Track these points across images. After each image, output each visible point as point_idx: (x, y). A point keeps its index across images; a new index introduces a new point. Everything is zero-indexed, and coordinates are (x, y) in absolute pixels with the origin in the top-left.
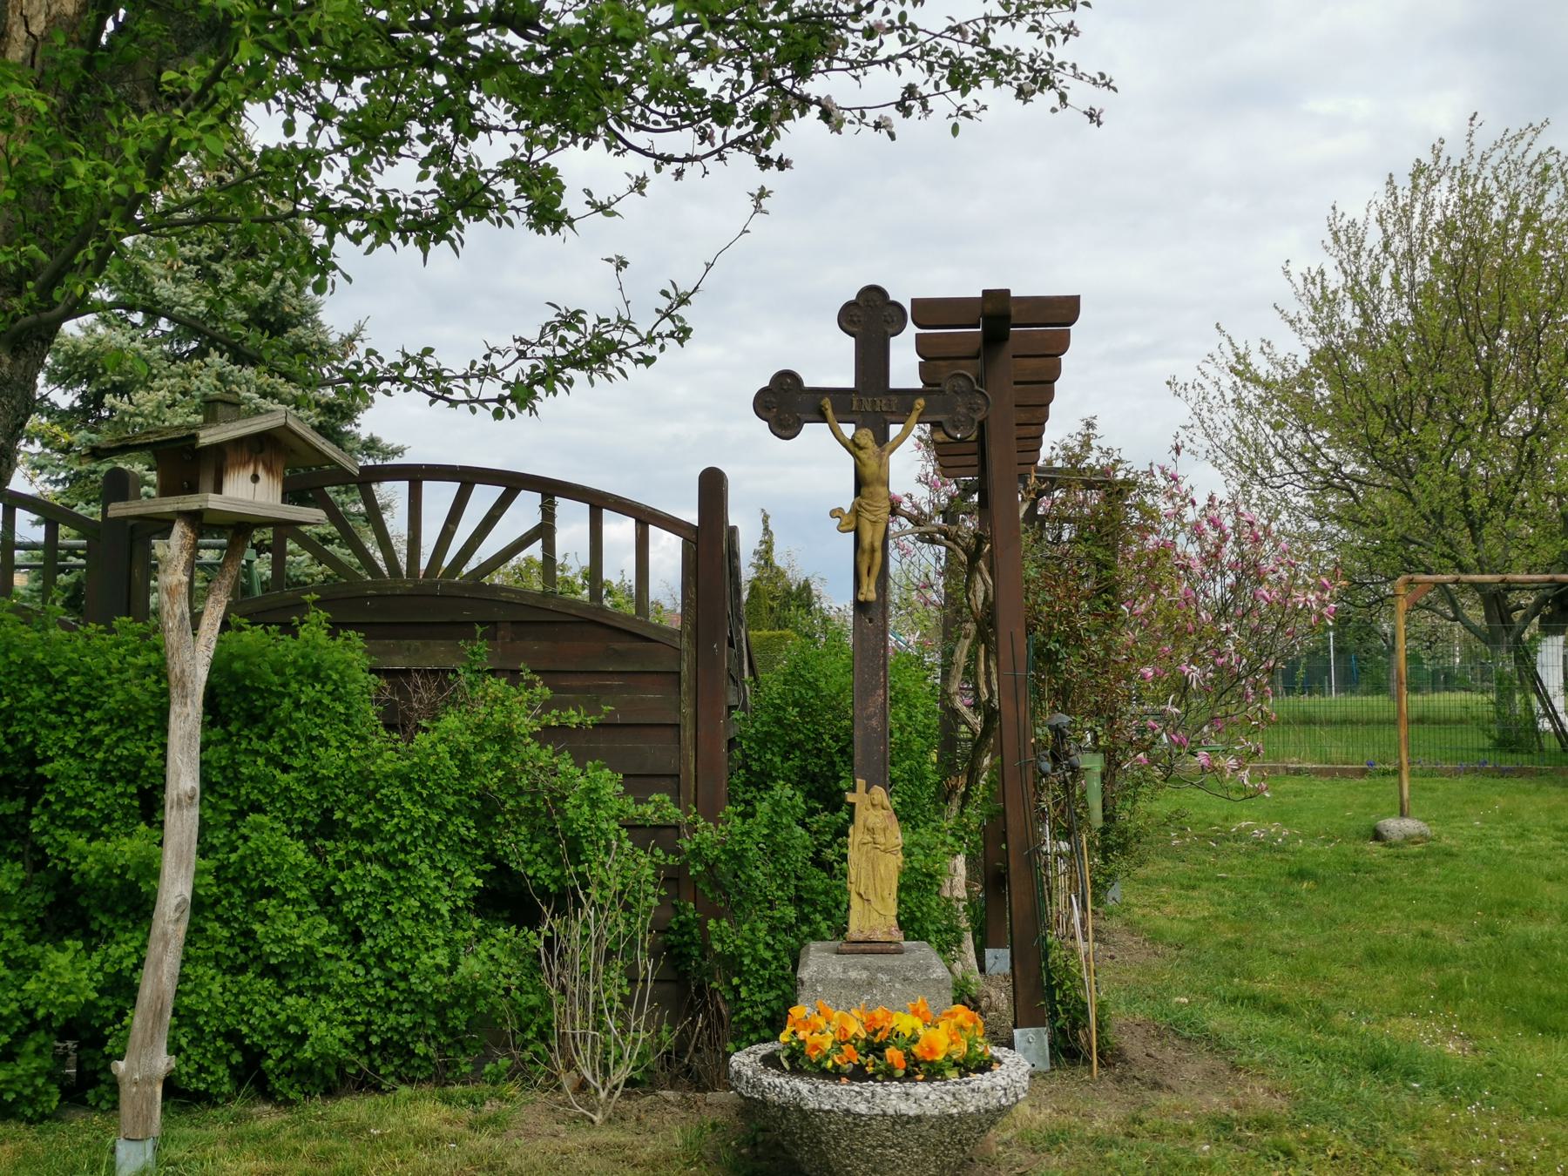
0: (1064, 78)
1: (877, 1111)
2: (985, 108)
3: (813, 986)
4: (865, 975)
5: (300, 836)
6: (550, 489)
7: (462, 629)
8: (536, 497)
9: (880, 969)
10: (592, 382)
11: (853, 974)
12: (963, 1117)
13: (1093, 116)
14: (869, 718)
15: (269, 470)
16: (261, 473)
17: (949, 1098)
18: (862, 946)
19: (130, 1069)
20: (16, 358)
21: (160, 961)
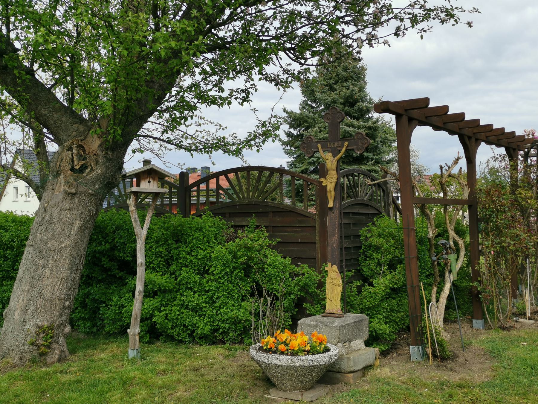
0: (457, 13)
2: (431, 28)
7: (249, 215)
9: (320, 322)
11: (312, 323)
12: (295, 367)
14: (333, 244)
15: (154, 179)
16: (151, 180)
18: (329, 315)
20: (113, 153)
21: (136, 305)
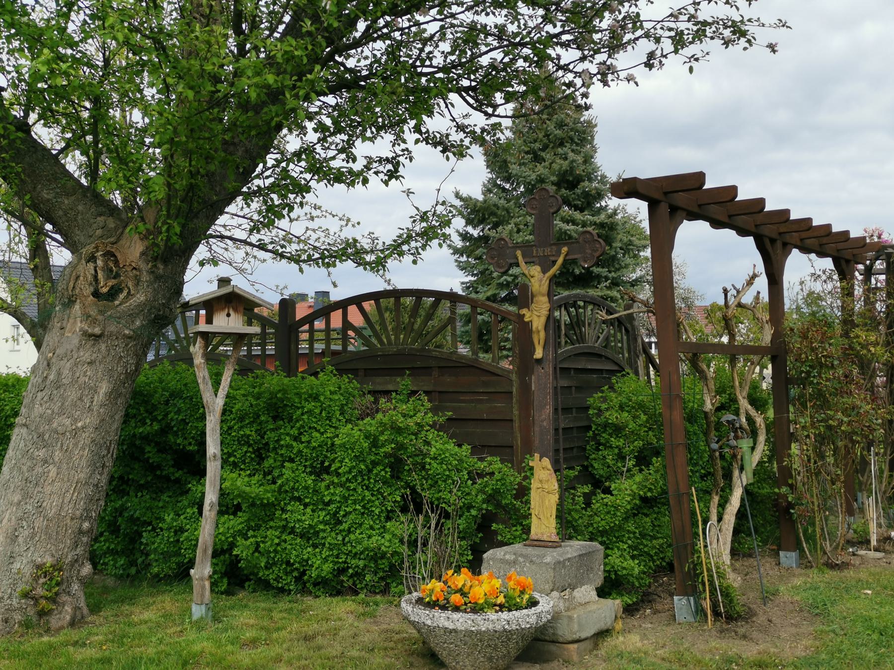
1: (435, 625)
2: (707, 54)
3: (488, 561)
4: (513, 557)
5: (311, 473)
9: (522, 555)
10: (301, 270)
11: (507, 557)
12: (479, 632)
13: (772, 48)
14: (542, 421)
15: (236, 310)
16: (232, 312)
17: (470, 622)
18: (535, 543)
19: (195, 573)
20: (166, 266)
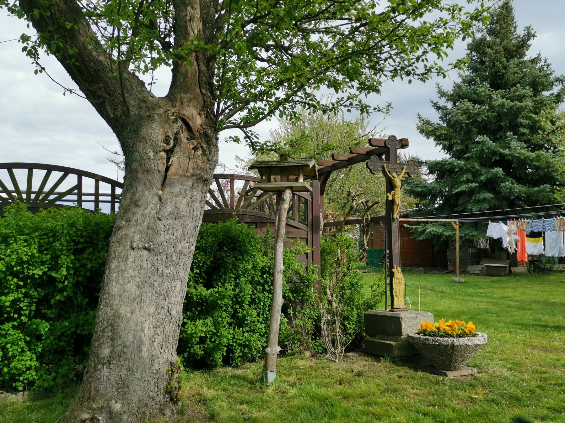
4: (415, 316)
6: (81, 174)
8: (76, 176)
